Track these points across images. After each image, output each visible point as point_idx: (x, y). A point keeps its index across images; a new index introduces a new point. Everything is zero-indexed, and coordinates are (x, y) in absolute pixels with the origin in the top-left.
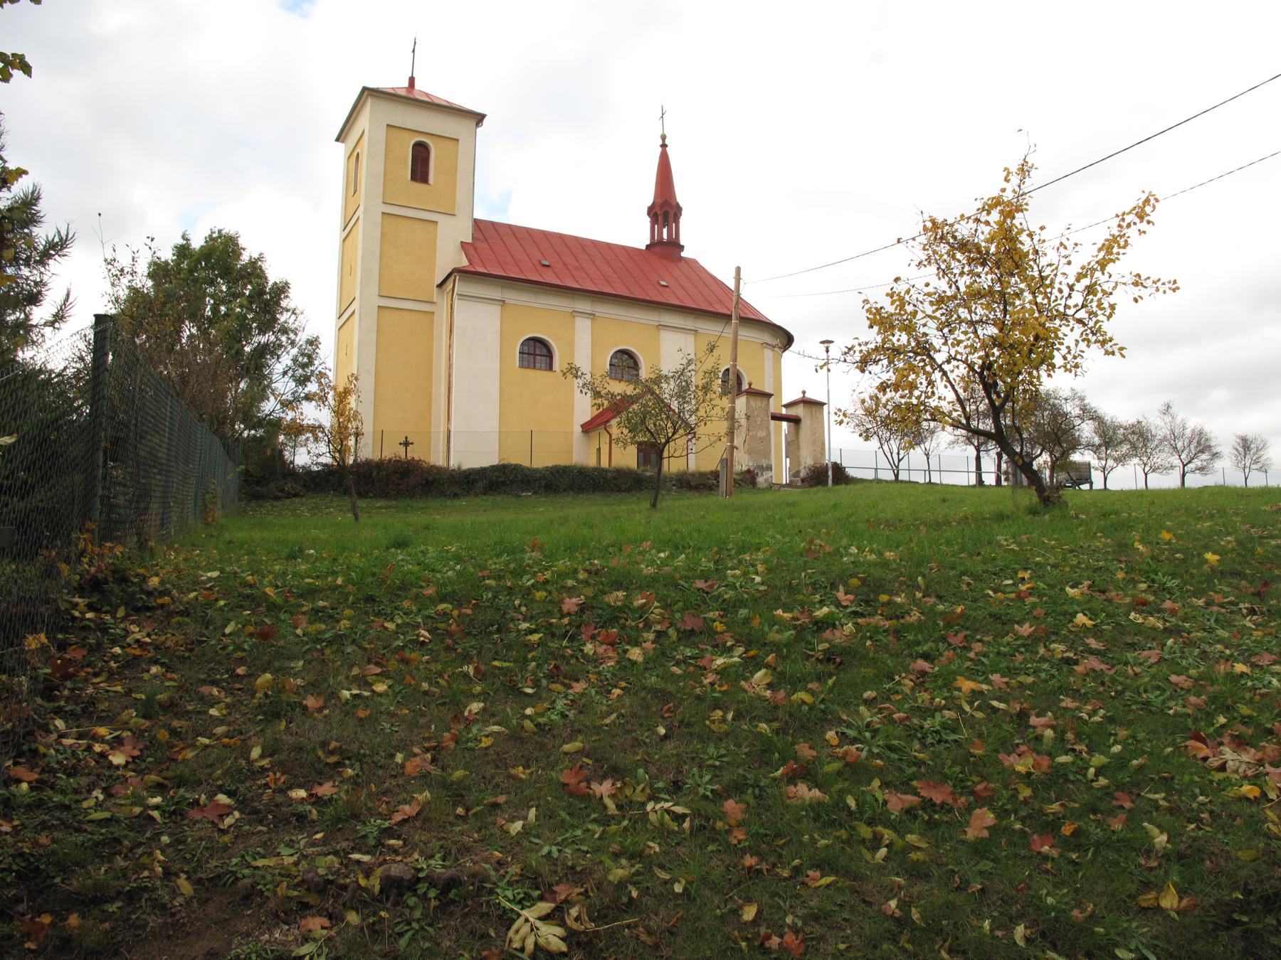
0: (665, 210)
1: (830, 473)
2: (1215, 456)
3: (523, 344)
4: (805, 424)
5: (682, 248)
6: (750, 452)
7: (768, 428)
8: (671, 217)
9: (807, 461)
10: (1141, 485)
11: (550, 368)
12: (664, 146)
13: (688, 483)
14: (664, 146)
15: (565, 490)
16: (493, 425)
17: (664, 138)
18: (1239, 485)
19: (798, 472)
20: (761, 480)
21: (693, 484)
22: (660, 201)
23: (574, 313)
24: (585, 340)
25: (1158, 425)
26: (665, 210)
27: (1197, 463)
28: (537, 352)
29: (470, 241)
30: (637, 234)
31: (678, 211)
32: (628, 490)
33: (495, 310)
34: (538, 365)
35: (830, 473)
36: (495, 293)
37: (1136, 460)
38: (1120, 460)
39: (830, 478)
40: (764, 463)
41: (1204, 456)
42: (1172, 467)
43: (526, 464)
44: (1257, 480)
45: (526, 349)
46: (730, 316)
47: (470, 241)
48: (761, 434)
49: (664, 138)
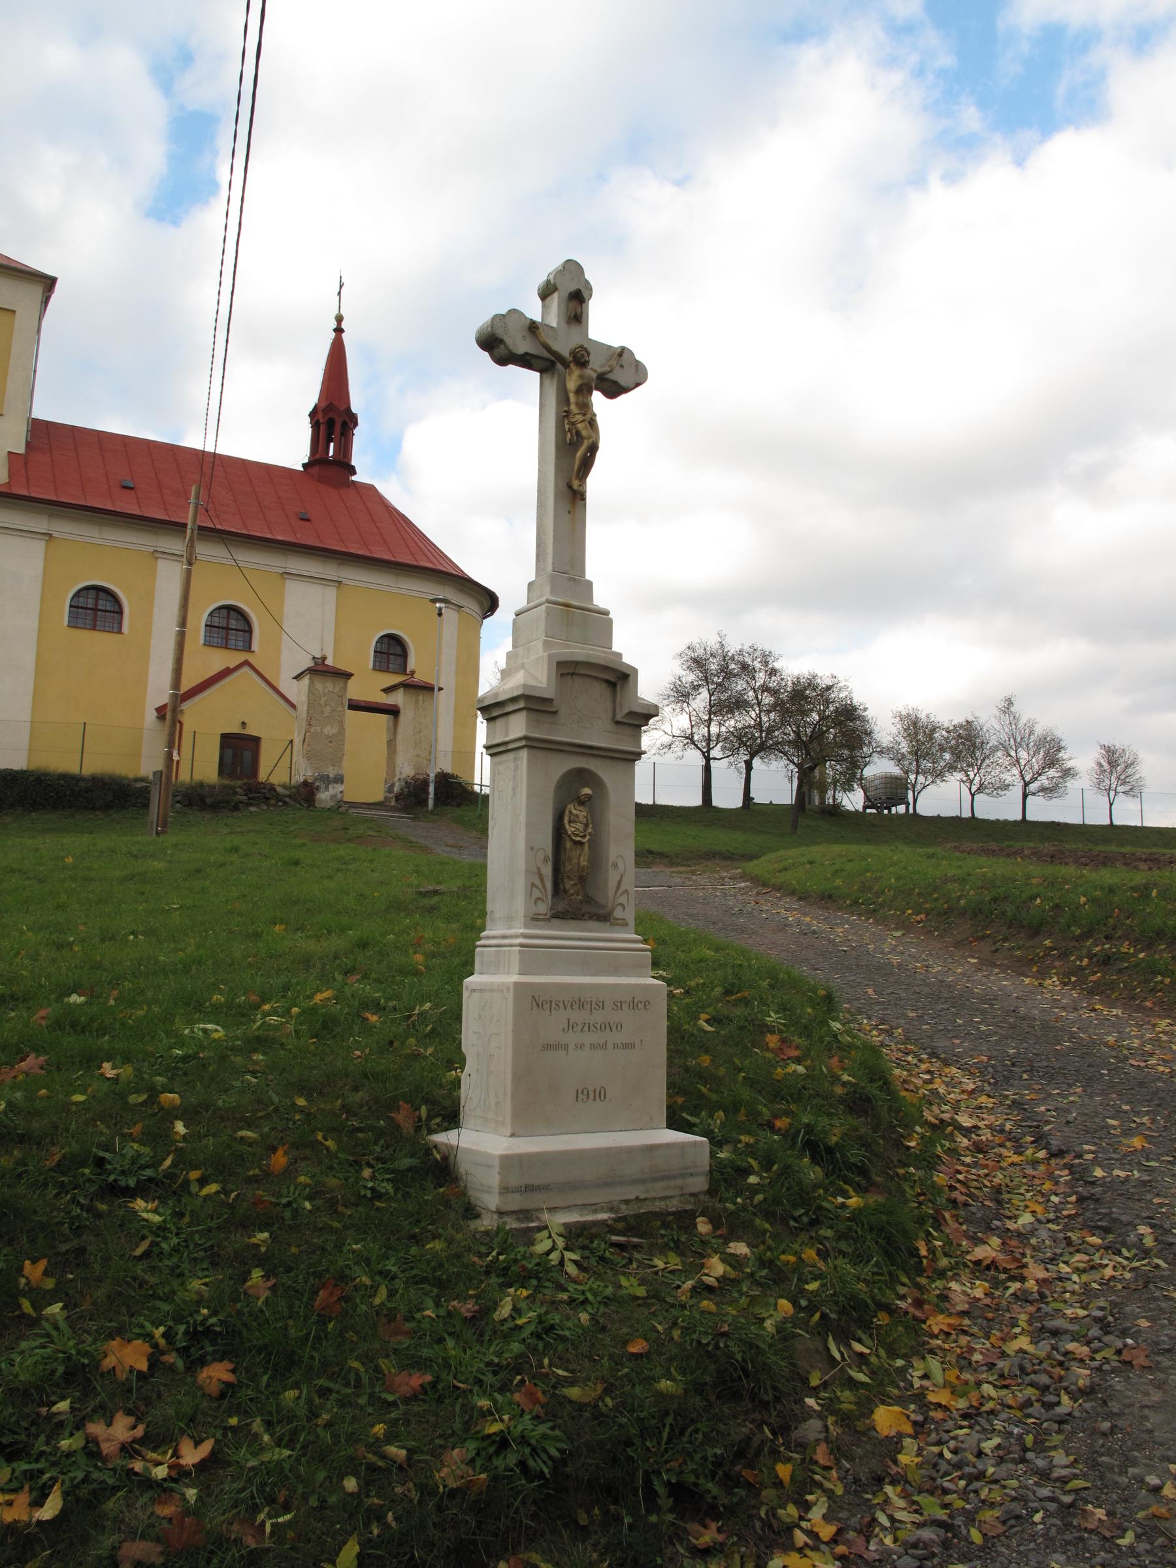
0: (333, 420)
1: (431, 789)
2: (1067, 773)
3: (211, 614)
4: (406, 716)
5: (353, 471)
6: (309, 756)
7: (341, 723)
8: (338, 428)
9: (406, 770)
10: (967, 814)
11: (120, 632)
12: (339, 331)
13: (202, 799)
14: (339, 331)
15: (12, 806)
16: (24, 715)
17: (339, 319)
18: (1011, 818)
19: (393, 785)
20: (324, 797)
21: (209, 800)
22: (323, 405)
23: (156, 554)
24: (162, 590)
25: (992, 725)
26: (333, 420)
27: (1043, 781)
28: (97, 608)
29: (21, 450)
30: (291, 448)
31: (350, 421)
32: (107, 807)
33: (331, 593)
34: (232, 643)
35: (431, 789)
36: (39, 523)
37: (959, 776)
38: (938, 775)
39: (431, 795)
40: (332, 772)
41: (1052, 773)
42: (1006, 787)
43: (73, 768)
44: (1128, 814)
45: (82, 601)
46: (185, 525)
47: (21, 450)
48: (329, 730)
49: (339, 319)
